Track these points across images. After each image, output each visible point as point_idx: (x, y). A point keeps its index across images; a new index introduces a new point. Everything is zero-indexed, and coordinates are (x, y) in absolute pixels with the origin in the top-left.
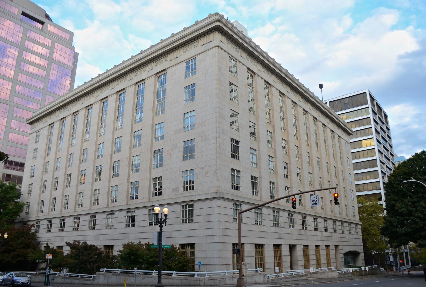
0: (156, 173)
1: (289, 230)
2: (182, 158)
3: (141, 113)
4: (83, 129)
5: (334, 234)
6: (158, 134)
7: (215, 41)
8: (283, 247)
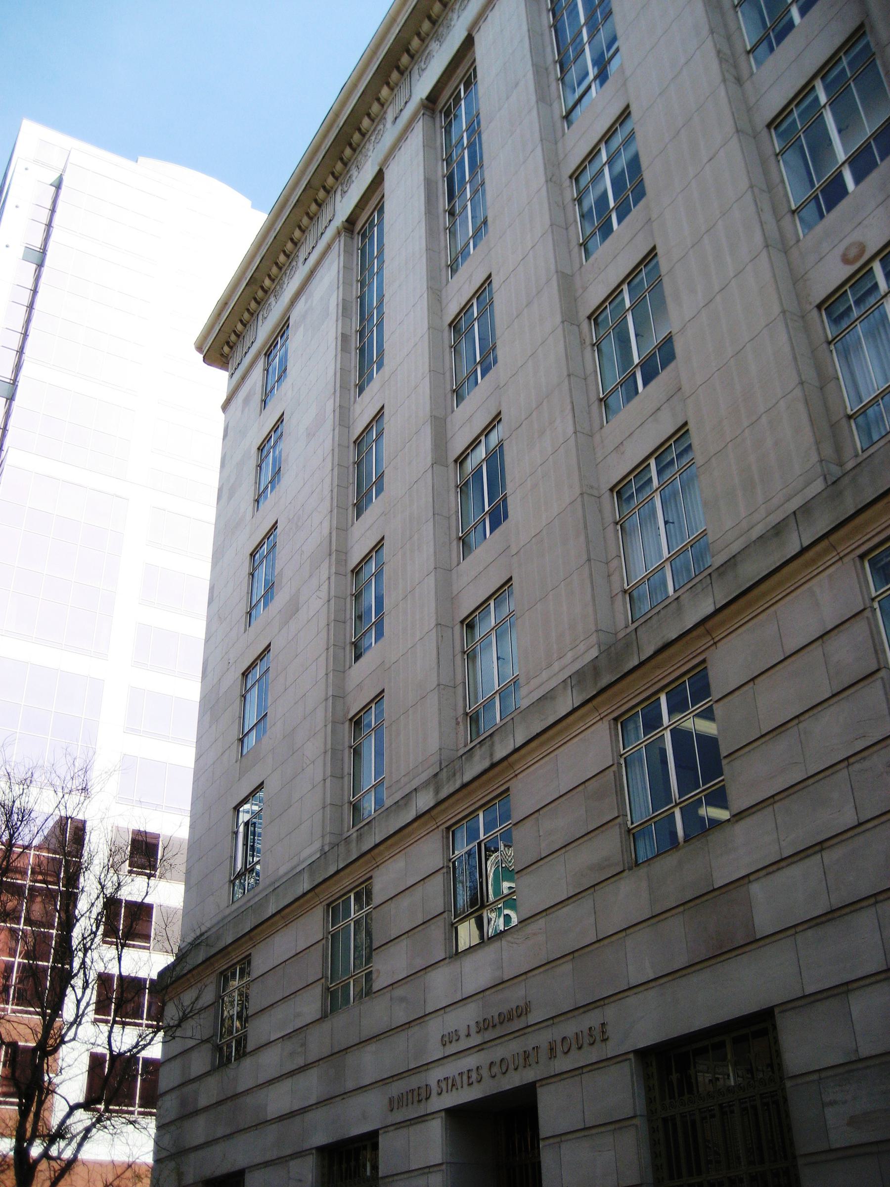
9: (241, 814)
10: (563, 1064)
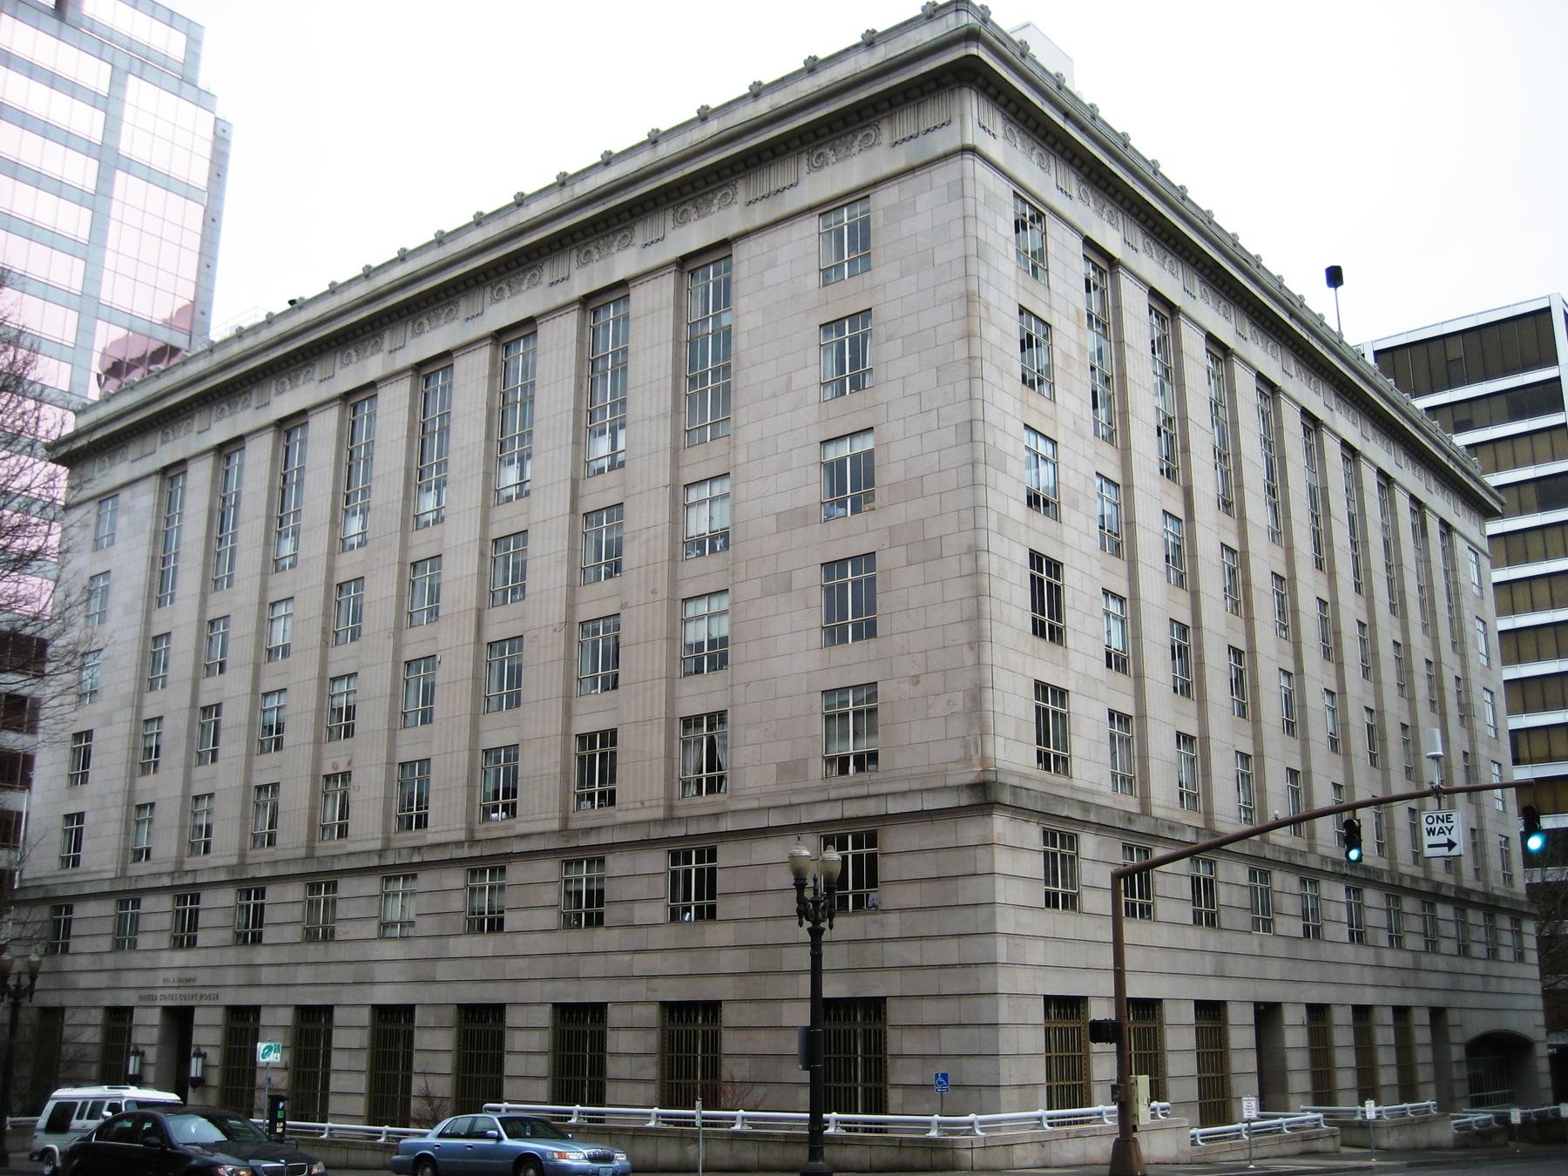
0: (593, 716)
1: (1252, 943)
2: (817, 637)
3: (521, 461)
4: (335, 494)
5: (1426, 960)
6: (699, 523)
7: (956, 125)
8: (1170, 1013)
9: (59, 412)
10: (204, 1002)
